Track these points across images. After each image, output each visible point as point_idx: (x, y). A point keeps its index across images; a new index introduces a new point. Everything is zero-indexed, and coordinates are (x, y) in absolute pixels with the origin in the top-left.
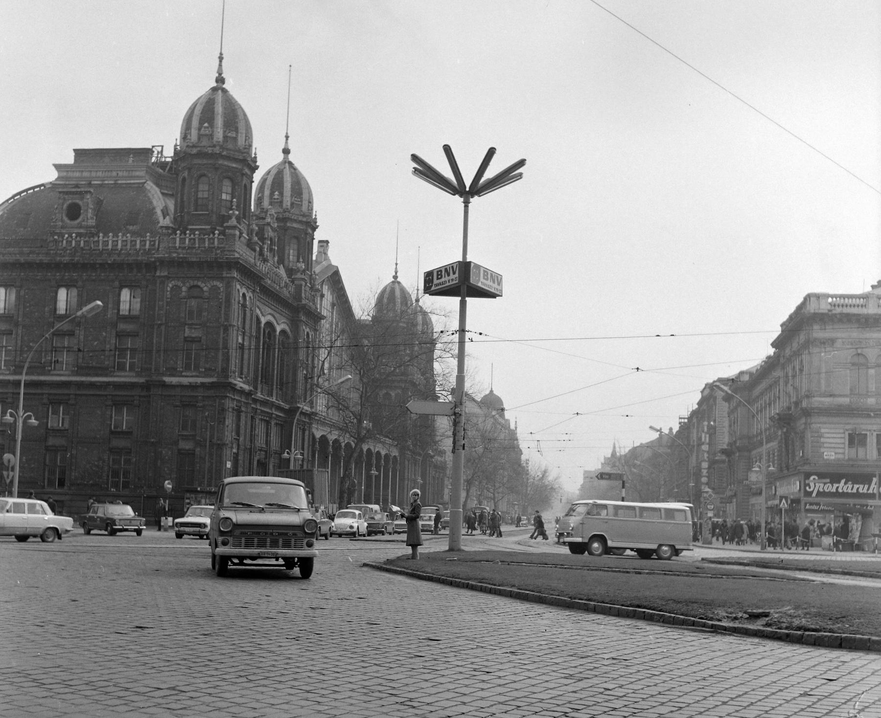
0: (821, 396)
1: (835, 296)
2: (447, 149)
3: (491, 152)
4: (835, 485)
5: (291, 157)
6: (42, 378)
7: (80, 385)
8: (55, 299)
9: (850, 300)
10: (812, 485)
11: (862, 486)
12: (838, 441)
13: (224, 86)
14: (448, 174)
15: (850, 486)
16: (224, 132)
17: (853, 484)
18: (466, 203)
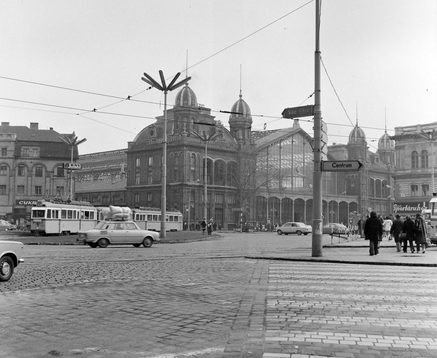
0: (400, 170)
2: (161, 73)
3: (178, 74)
4: (404, 208)
5: (243, 98)
6: (146, 186)
7: (154, 187)
8: (148, 161)
10: (395, 208)
11: (414, 208)
13: (188, 86)
14: (161, 85)
15: (410, 208)
16: (183, 102)
18: (166, 93)
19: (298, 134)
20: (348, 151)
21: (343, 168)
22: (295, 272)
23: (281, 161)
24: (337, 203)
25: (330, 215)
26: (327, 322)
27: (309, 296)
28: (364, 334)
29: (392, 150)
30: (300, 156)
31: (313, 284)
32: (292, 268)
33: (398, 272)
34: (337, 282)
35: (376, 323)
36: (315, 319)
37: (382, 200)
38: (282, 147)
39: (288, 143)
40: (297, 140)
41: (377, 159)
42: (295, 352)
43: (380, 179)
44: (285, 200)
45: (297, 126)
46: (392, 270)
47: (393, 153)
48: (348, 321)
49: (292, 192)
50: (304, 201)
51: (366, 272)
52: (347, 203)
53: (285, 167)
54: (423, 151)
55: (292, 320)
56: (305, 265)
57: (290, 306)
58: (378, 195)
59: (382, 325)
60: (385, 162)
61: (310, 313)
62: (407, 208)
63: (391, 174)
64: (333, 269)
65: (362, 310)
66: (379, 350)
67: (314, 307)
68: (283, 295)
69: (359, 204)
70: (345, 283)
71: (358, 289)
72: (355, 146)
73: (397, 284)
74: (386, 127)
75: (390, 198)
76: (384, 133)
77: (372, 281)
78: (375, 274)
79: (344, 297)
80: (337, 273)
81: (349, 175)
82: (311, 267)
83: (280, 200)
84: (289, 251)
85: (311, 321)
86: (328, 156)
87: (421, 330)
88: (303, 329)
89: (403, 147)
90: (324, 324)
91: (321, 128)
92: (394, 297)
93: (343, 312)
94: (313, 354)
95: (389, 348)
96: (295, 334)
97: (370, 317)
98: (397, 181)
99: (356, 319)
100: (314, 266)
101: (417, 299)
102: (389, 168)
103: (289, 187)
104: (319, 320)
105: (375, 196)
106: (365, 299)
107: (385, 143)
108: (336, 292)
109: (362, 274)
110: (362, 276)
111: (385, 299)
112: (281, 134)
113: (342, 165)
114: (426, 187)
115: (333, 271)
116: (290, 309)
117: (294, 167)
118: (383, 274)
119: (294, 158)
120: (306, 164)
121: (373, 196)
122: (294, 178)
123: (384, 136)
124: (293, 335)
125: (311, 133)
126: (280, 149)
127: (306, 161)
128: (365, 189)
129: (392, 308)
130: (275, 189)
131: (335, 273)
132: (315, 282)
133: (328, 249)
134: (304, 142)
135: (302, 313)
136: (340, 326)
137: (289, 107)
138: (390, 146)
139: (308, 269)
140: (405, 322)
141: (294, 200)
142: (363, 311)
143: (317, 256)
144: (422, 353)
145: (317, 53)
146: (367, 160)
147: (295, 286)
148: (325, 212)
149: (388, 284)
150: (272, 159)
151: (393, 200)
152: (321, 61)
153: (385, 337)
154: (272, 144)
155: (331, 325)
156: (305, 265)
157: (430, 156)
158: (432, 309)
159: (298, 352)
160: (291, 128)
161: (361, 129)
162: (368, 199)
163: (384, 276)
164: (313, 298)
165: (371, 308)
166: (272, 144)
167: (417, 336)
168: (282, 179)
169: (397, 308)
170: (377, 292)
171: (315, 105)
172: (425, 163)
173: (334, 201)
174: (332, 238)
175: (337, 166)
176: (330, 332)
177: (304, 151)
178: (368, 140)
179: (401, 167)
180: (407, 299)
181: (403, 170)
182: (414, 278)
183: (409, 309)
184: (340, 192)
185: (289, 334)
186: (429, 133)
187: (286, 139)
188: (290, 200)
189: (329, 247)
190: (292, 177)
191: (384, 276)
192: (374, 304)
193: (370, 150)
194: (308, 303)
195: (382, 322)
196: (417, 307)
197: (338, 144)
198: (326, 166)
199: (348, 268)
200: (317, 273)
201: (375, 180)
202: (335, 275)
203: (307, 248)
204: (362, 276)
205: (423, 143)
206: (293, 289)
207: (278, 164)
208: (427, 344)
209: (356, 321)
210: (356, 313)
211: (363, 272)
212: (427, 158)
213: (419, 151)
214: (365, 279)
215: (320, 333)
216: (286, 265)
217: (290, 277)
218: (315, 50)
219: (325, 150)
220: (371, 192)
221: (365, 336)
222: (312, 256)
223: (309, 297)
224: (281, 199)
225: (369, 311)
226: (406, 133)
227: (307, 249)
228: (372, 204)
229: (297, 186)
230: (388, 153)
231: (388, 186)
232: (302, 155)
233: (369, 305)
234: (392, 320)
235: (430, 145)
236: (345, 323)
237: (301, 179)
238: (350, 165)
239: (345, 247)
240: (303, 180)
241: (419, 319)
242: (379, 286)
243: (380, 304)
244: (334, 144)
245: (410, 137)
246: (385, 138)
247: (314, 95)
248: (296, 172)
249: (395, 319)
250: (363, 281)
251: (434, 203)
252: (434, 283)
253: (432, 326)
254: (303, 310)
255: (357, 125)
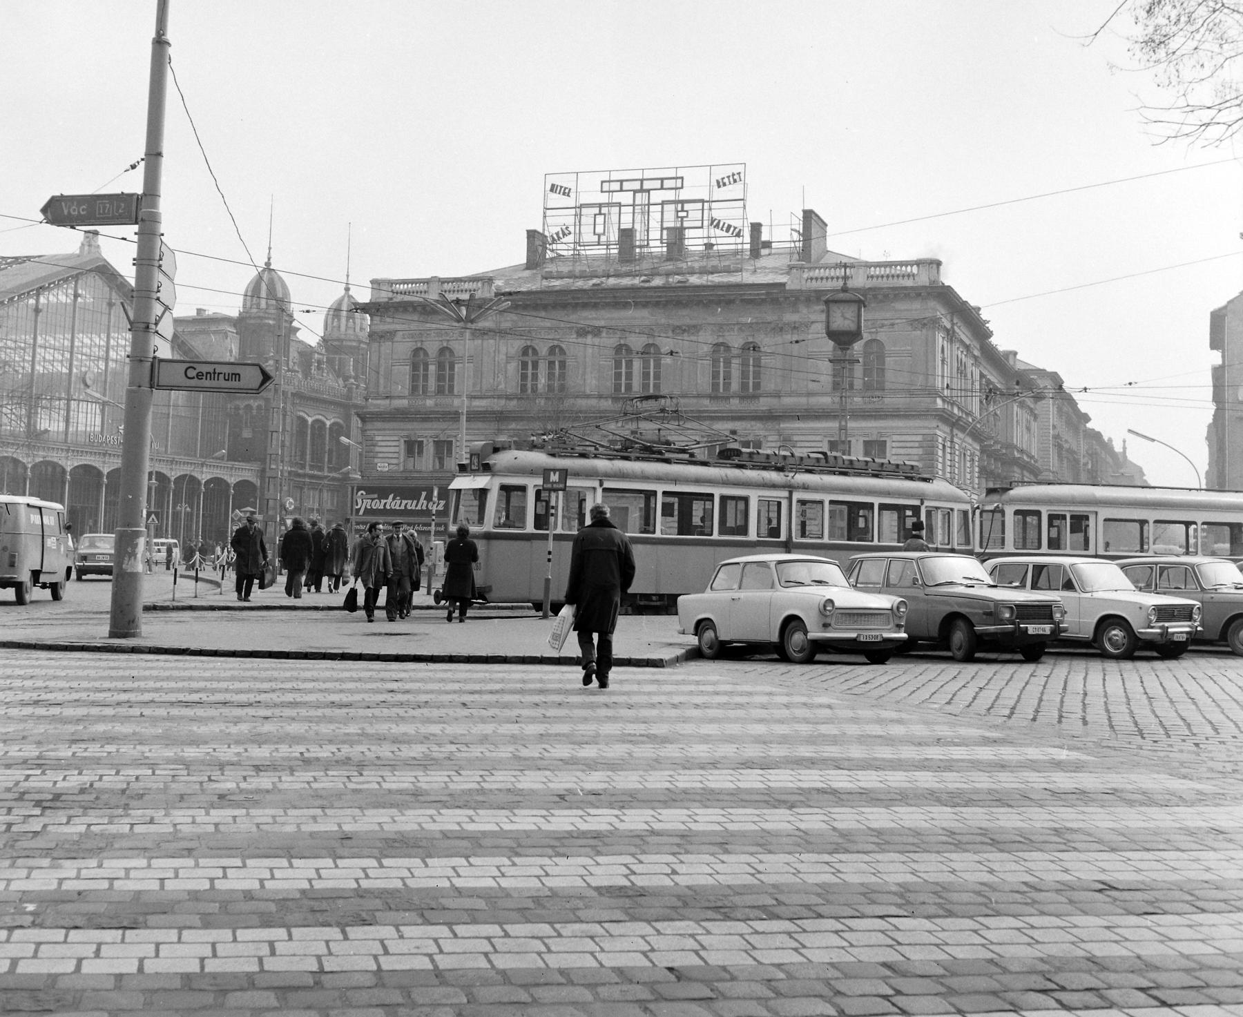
1: (405, 282)
4: (383, 501)
9: (904, 268)
10: (360, 501)
11: (410, 502)
12: (392, 449)
15: (399, 502)
17: (401, 499)
19: (93, 274)
20: (238, 337)
21: (214, 383)
22: (52, 684)
23: (38, 350)
24: (199, 483)
25: (176, 515)
26: (131, 829)
27: (85, 754)
28: (237, 857)
29: (360, 342)
30: (97, 340)
31: (102, 719)
32: (43, 672)
33: (352, 680)
34: (175, 711)
35: (275, 822)
36: (97, 822)
37: (327, 477)
38: (41, 311)
39: (63, 298)
40: (91, 293)
41: (319, 362)
42: (25, 924)
43: (306, 416)
44: (43, 467)
45: (93, 249)
46: (335, 674)
47: (363, 349)
48: (193, 822)
49: (69, 447)
50: (100, 474)
51: (263, 680)
52: (228, 485)
53: (47, 369)
54: (443, 351)
55: (26, 828)
56: (86, 663)
57: (26, 784)
58: (317, 463)
59: (290, 829)
60: (340, 373)
61: (83, 803)
62: (392, 503)
63: (356, 406)
64: (167, 673)
65: (239, 787)
66: (273, 901)
67: (96, 785)
68: (7, 752)
69: (262, 487)
70: (200, 712)
71: (234, 730)
72: (259, 321)
73: (345, 710)
74: (348, 276)
75: (348, 473)
76: (343, 292)
77: (276, 705)
78: (289, 685)
79: (191, 752)
80: (180, 685)
81: (237, 402)
82: (104, 669)
83: (25, 468)
84: (42, 622)
85: (83, 828)
86: (177, 342)
87: (395, 837)
88: (55, 854)
89: (388, 336)
90: (122, 836)
91: (156, 264)
92: (333, 748)
93: (182, 797)
94: (79, 925)
95: (303, 892)
96: (31, 869)
97: (260, 808)
98: (369, 426)
99: (217, 815)
100: (112, 664)
101: (393, 752)
102: (350, 390)
103: (56, 429)
104: (110, 823)
105: (307, 467)
106: (249, 758)
107: (343, 320)
108: (168, 740)
109: (252, 685)
110: (249, 691)
111: (306, 755)
112: (42, 272)
113: (214, 373)
114: (444, 447)
115: (168, 679)
116: (24, 793)
117: (75, 370)
118: (310, 685)
119: (76, 344)
120: (112, 365)
121: (303, 467)
122: (73, 404)
123: (340, 302)
124: (24, 873)
125: (129, 273)
126: (37, 316)
127: (112, 354)
128: (280, 442)
129: (324, 779)
130: (12, 434)
131: (172, 685)
132: (109, 711)
133: (160, 614)
134: (110, 299)
135: (59, 804)
136: (170, 838)
137: (65, 194)
138: (358, 329)
139: (92, 673)
140: (354, 817)
141: (69, 469)
142: (241, 791)
143: (125, 636)
144: (389, 901)
145: (160, 43)
146: (291, 364)
147: (48, 727)
148: (162, 507)
149: (319, 712)
150: (9, 343)
151: (355, 479)
152: (169, 69)
153: (296, 862)
154: (11, 299)
155: (144, 836)
156: (86, 663)
157: (461, 365)
158: (429, 779)
159: (33, 922)
160: (72, 255)
161: (280, 278)
162: (286, 474)
163: (311, 691)
164: (99, 758)
165: (265, 781)
166: (11, 299)
167: (381, 853)
168: (36, 406)
169: (336, 779)
170: (288, 734)
171: (145, 194)
172: (445, 381)
173: (191, 476)
174: (175, 583)
175: (197, 375)
176: (138, 856)
177: (109, 326)
178: (295, 309)
179: (381, 389)
180: (367, 753)
181: (387, 397)
182: (391, 694)
183: (370, 779)
184: (209, 451)
185: (12, 870)
186: (458, 302)
187: (58, 286)
188: (58, 469)
189: (164, 609)
190: (69, 400)
191: (311, 691)
192: (275, 769)
193: (300, 335)
194: (80, 774)
195: (291, 820)
196: (390, 774)
197: (210, 313)
198: (165, 376)
199: (211, 669)
200: (120, 685)
201: (310, 420)
202: (172, 691)
203: (97, 613)
204: (249, 691)
205: (442, 327)
206: (42, 734)
207: (27, 358)
208: (406, 874)
209: (217, 820)
210: (221, 797)
211: (255, 679)
212: (452, 368)
213: (432, 347)
214: (258, 699)
215: (106, 863)
216: (27, 662)
217: (36, 698)
218: (153, 34)
219: (166, 328)
220: (299, 453)
221: (238, 862)
222: (110, 637)
223: (85, 758)
224: (30, 466)
225: (258, 791)
226: (399, 298)
227: (98, 616)
228: (300, 487)
229: (81, 428)
230: (351, 347)
231: (344, 439)
232: (104, 336)
233: (262, 774)
234: (319, 811)
235: (462, 334)
236: (186, 829)
237: (97, 408)
238: (237, 376)
239: (212, 608)
240: (103, 411)
241: (392, 806)
242: (293, 719)
243: (292, 771)
244: (199, 311)
245: (411, 309)
246: (345, 307)
247: (143, 164)
248: (82, 386)
249: (327, 810)
250: (251, 705)
251: (460, 490)
252: (444, 707)
253: (424, 825)
254: (63, 798)
255: (268, 264)
